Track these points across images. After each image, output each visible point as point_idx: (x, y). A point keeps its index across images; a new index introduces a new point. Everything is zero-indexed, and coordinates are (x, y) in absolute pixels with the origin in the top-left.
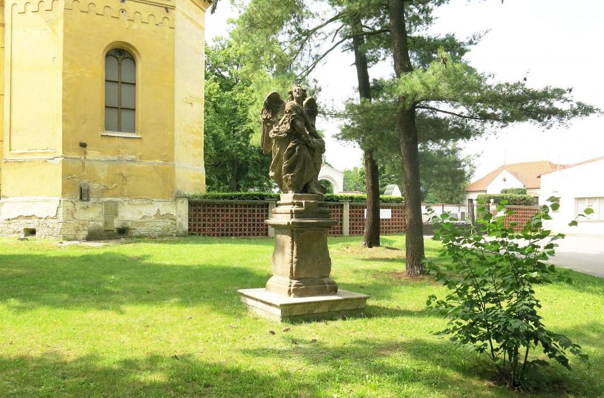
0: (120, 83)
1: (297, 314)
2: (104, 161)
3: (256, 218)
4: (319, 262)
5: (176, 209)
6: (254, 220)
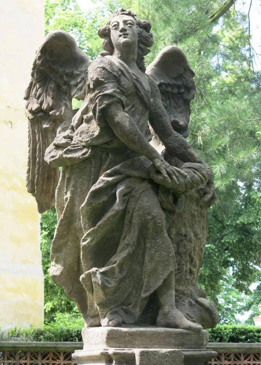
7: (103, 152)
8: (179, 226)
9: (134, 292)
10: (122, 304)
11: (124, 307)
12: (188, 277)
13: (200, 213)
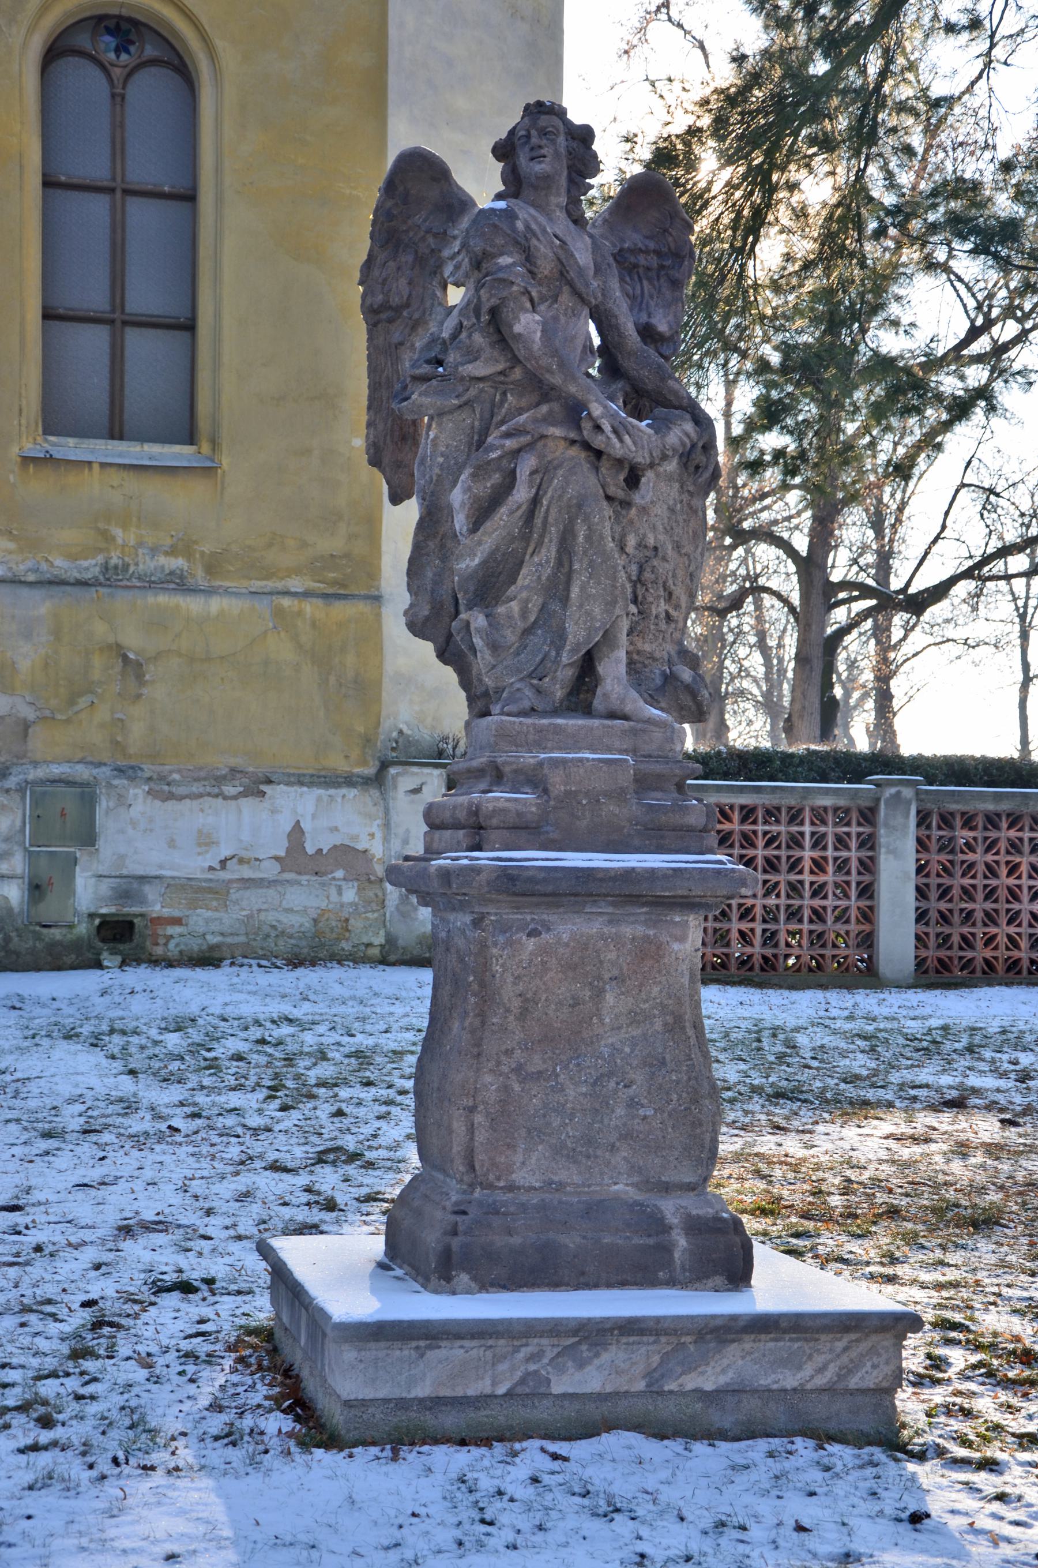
0: (119, 194)
1: (445, 1392)
2: (30, 584)
3: (807, 878)
4: (632, 1104)
5: (387, 825)
6: (795, 889)
7: (496, 388)
8: (641, 531)
9: (553, 653)
10: (530, 676)
11: (535, 682)
12: (663, 626)
13: (689, 504)
